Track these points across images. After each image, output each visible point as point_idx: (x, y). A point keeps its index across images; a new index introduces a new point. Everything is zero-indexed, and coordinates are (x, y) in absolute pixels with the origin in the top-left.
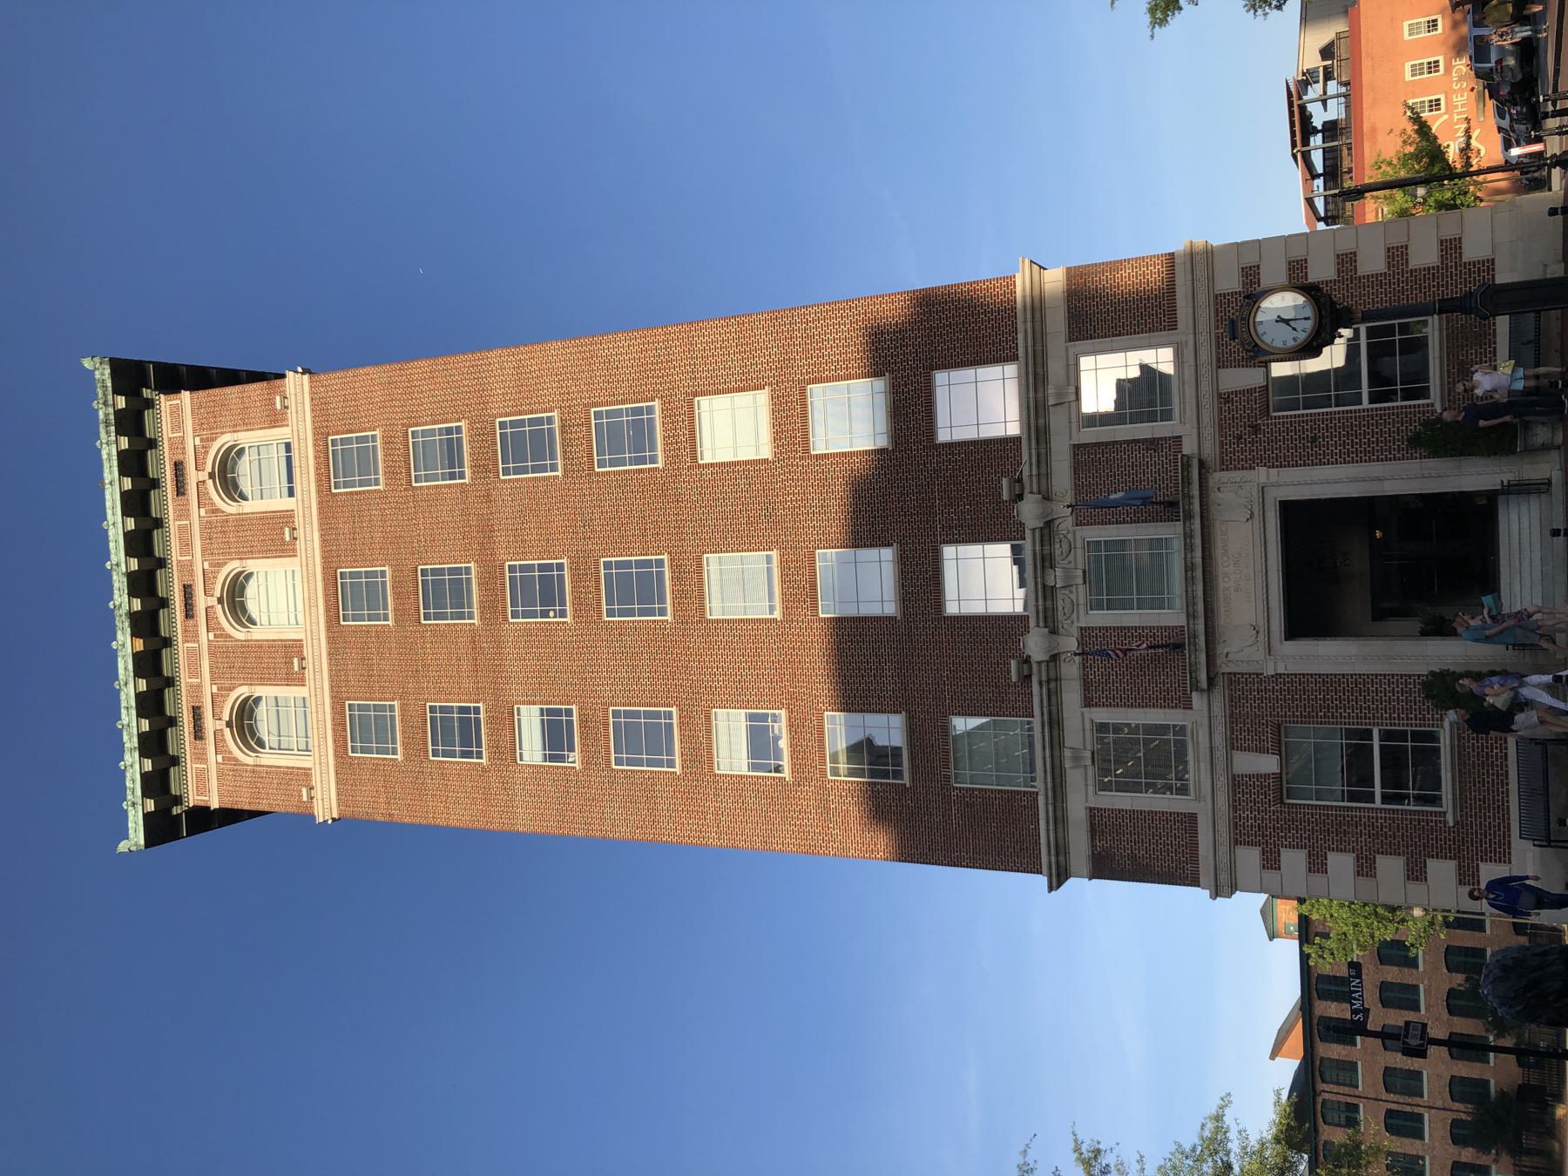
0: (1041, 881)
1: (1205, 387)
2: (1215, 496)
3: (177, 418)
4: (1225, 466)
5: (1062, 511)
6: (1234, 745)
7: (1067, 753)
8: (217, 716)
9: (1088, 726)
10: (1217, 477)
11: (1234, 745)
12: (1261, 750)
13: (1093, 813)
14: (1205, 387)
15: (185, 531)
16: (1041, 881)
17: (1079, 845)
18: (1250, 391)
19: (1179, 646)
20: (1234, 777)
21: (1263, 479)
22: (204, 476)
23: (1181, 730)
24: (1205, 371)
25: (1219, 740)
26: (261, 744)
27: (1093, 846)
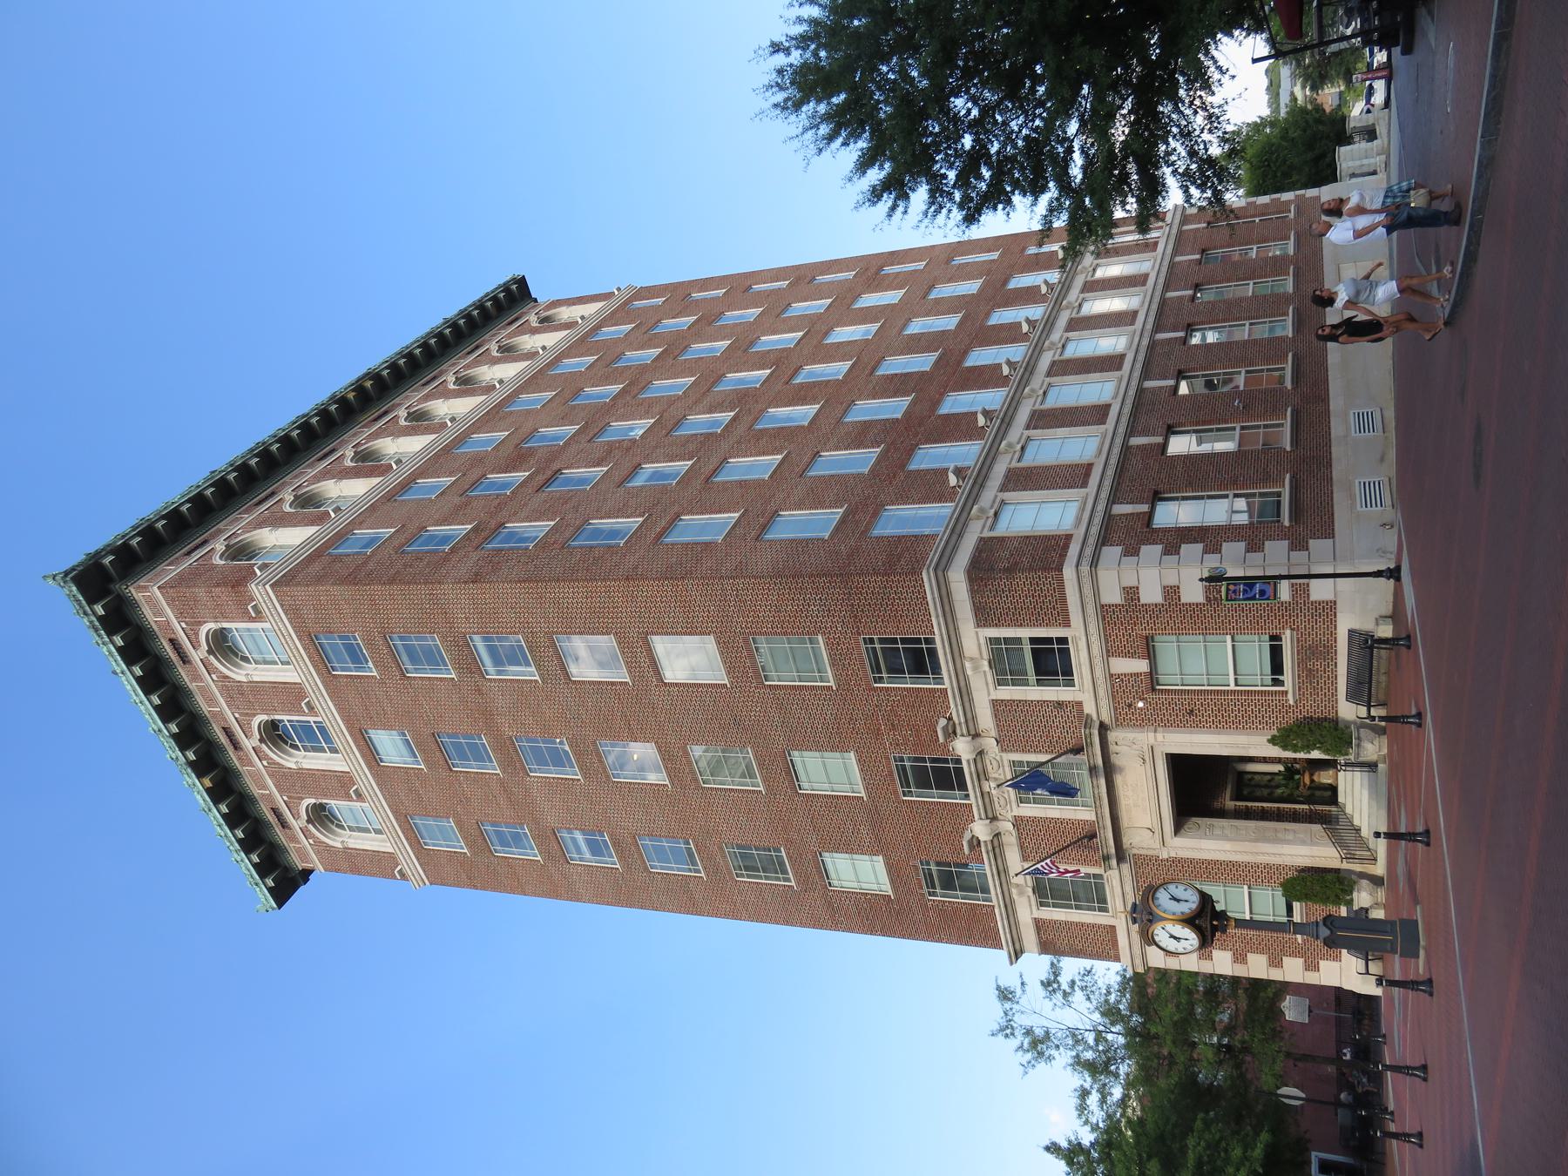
0: (1002, 955)
1: (1099, 673)
2: (1113, 748)
3: (152, 597)
4: (1120, 722)
5: (990, 744)
6: (1110, 652)
7: (968, 665)
8: (296, 816)
9: (982, 641)
10: (1112, 736)
11: (1110, 652)
12: (1132, 655)
13: (996, 705)
14: (1099, 673)
15: (205, 691)
16: (1002, 955)
17: (1029, 937)
18: (1137, 675)
19: (1093, 836)
20: (1111, 676)
21: (1152, 741)
22: (255, 741)
23: (1063, 641)
24: (1098, 661)
25: (1096, 650)
26: (245, 659)
27: (1040, 938)
